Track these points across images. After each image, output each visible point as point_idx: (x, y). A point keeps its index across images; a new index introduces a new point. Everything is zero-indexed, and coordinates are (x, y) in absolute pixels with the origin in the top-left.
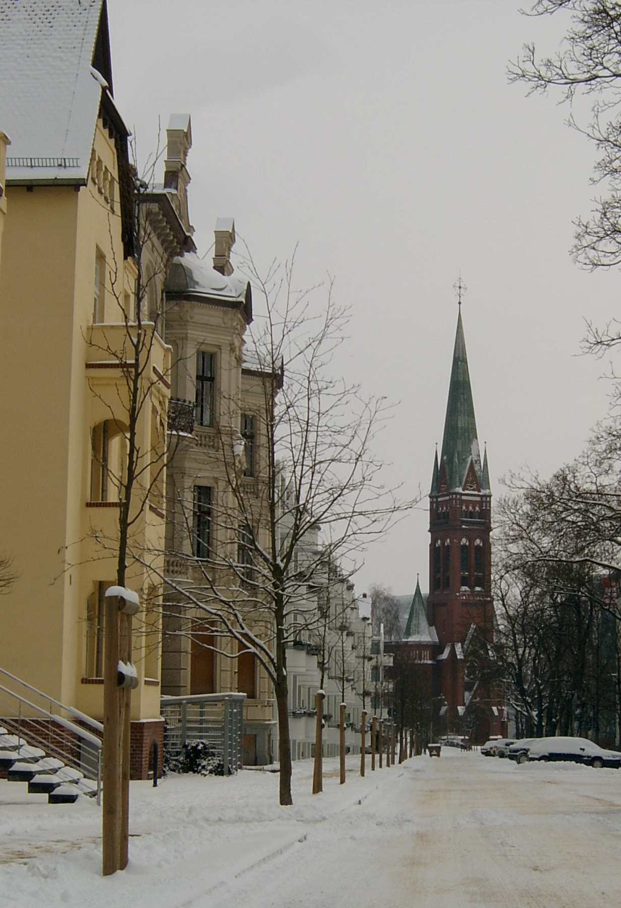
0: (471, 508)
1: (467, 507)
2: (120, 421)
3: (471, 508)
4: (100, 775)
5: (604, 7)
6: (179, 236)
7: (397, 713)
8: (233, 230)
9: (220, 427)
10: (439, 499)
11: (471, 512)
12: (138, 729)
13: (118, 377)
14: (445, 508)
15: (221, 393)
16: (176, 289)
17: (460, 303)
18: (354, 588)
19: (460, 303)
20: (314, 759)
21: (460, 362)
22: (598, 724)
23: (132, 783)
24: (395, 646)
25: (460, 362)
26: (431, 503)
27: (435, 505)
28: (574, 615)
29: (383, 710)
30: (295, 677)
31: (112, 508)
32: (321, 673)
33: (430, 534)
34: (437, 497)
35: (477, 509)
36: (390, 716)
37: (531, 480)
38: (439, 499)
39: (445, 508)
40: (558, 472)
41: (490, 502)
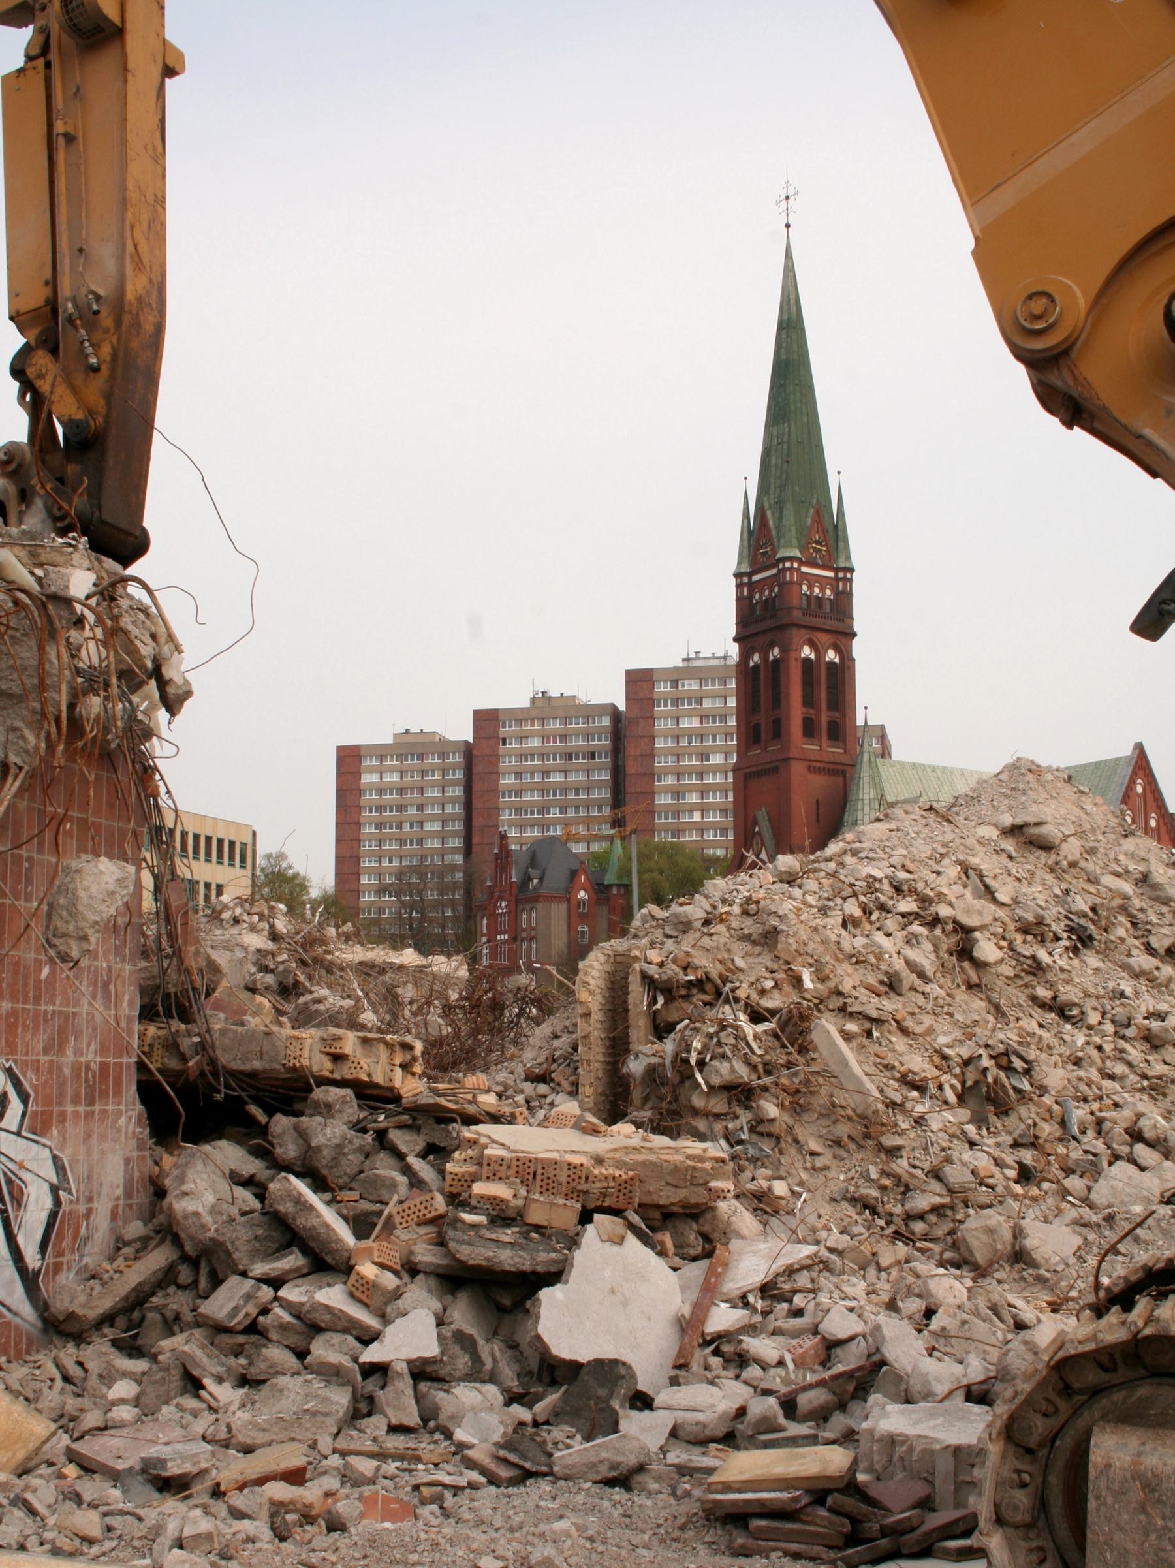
0: (816, 590)
1: (811, 588)
2: (641, 1410)
3: (816, 590)
4: (587, 1091)
5: (26, 1362)
6: (43, 745)
7: (82, 343)
8: (123, 21)
9: (540, 906)
10: (755, 578)
11: (817, 597)
12: (512, 883)
13: (115, 1408)
14: (767, 593)
15: (686, 1198)
16: (1130, 769)
17: (788, 226)
18: (647, 1413)
19: (788, 226)
20: (527, 704)
21: (788, 256)
22: (938, 957)
23: (167, 81)
24: (613, 1055)
25: (788, 256)
26: (739, 586)
27: (745, 590)
28: (218, 932)
29: (863, 724)
30: (232, 1243)
31: (47, 176)
32: (721, 1435)
33: (736, 645)
34: (750, 575)
35: (828, 592)
36: (401, 1278)
37: (874, 1513)
38: (755, 578)
39: (767, 593)
40: (987, 1369)
41: (851, 580)
